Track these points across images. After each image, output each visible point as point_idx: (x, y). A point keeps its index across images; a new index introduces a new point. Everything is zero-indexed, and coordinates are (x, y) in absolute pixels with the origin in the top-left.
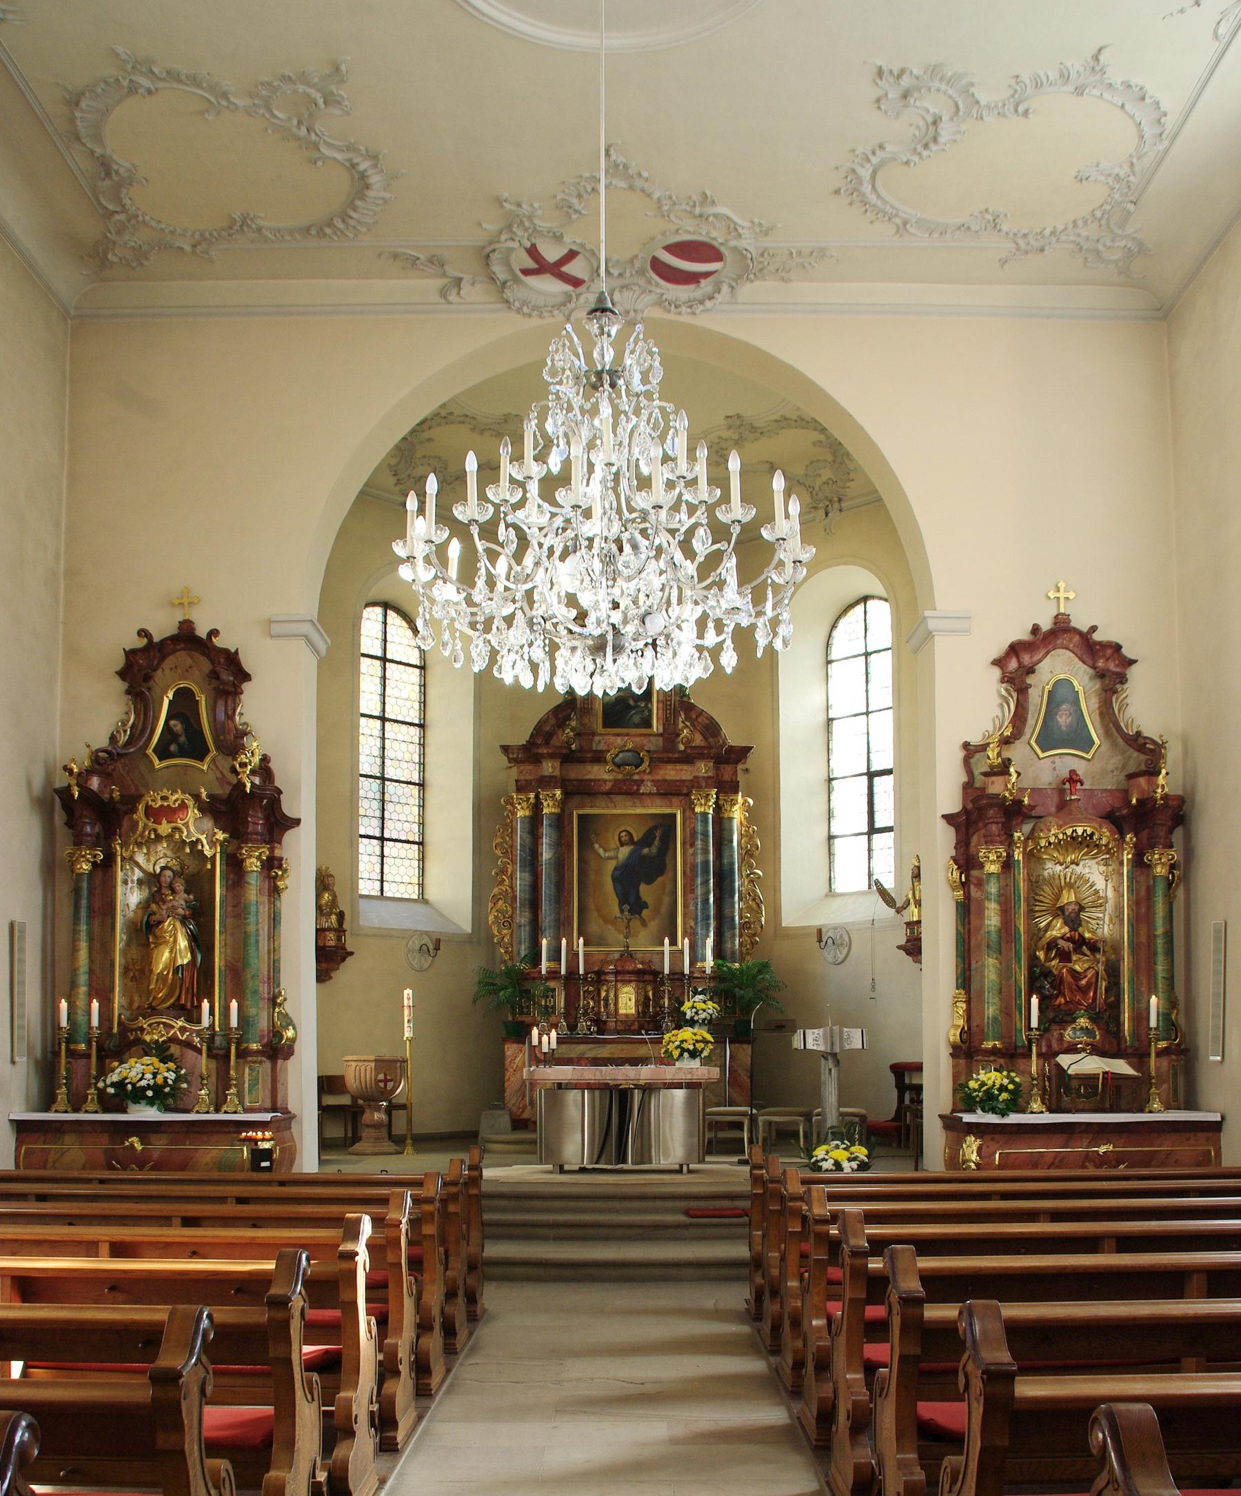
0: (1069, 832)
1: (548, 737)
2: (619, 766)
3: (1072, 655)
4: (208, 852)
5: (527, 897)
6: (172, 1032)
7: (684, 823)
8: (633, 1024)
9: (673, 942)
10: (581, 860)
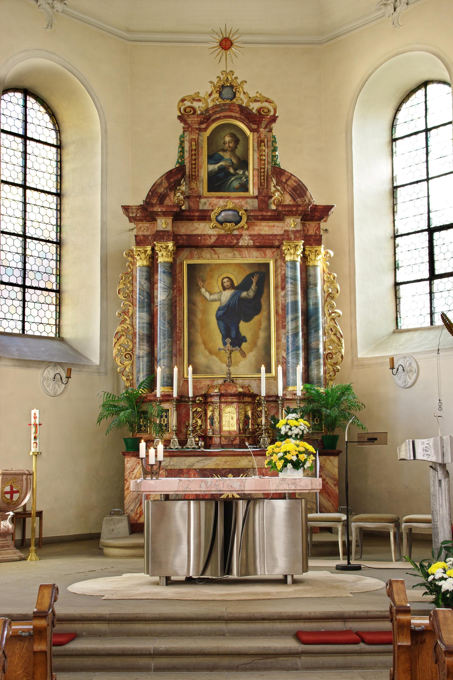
1: (162, 198)
2: (221, 223)
5: (145, 332)
7: (276, 271)
8: (235, 439)
9: (268, 370)
10: (191, 302)
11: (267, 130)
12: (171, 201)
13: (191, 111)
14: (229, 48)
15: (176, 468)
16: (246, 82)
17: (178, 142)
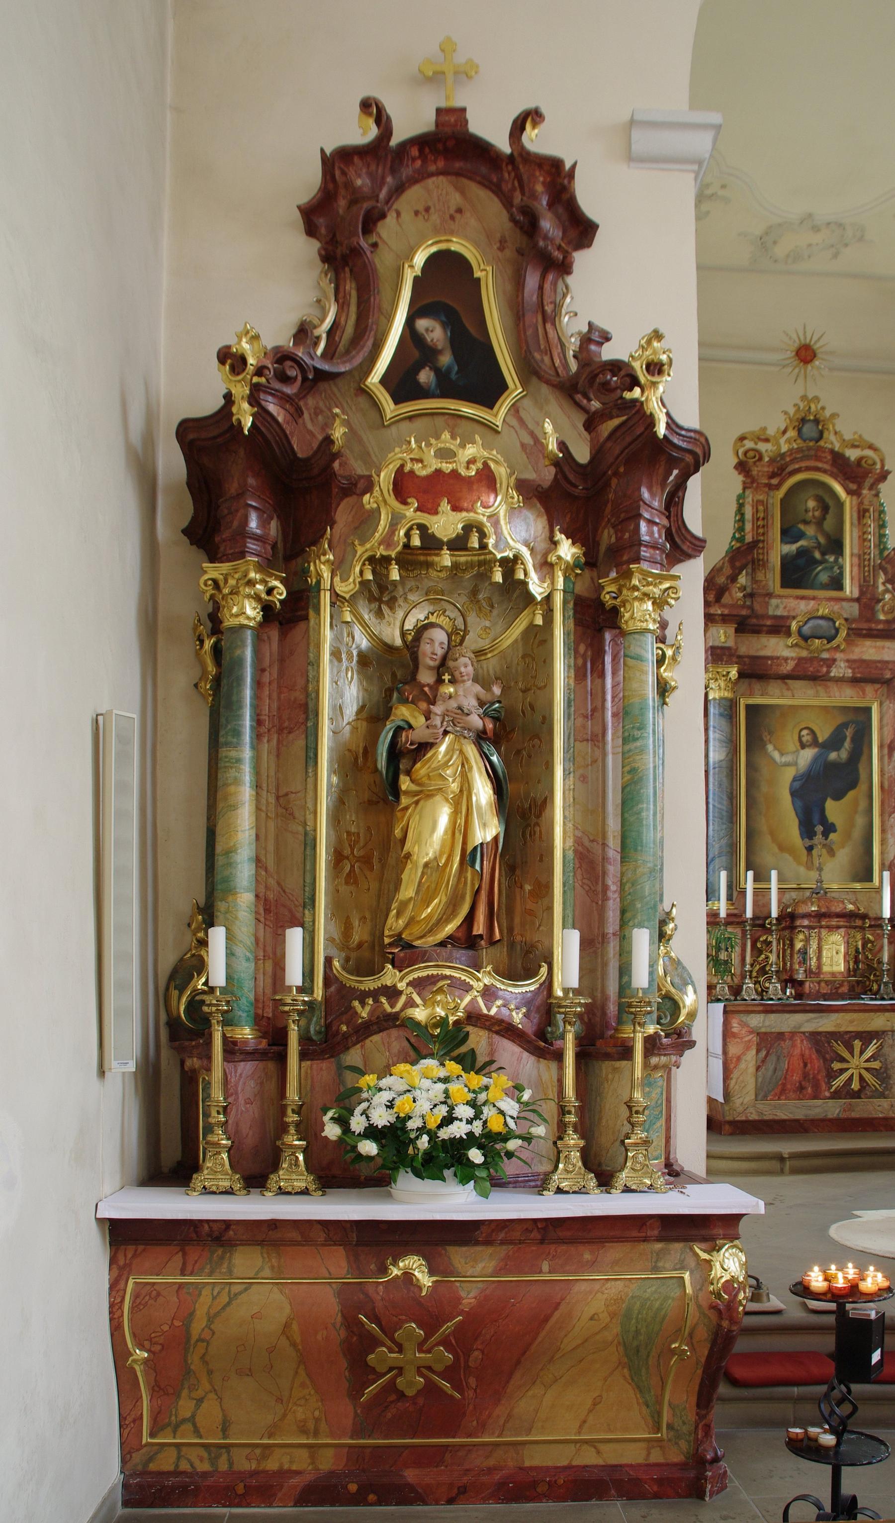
2: (806, 639)
4: (537, 588)
6: (468, 999)
10: (750, 765)
11: (873, 492)
12: (732, 598)
13: (755, 457)
14: (811, 361)
15: (773, 1030)
17: (734, 507)
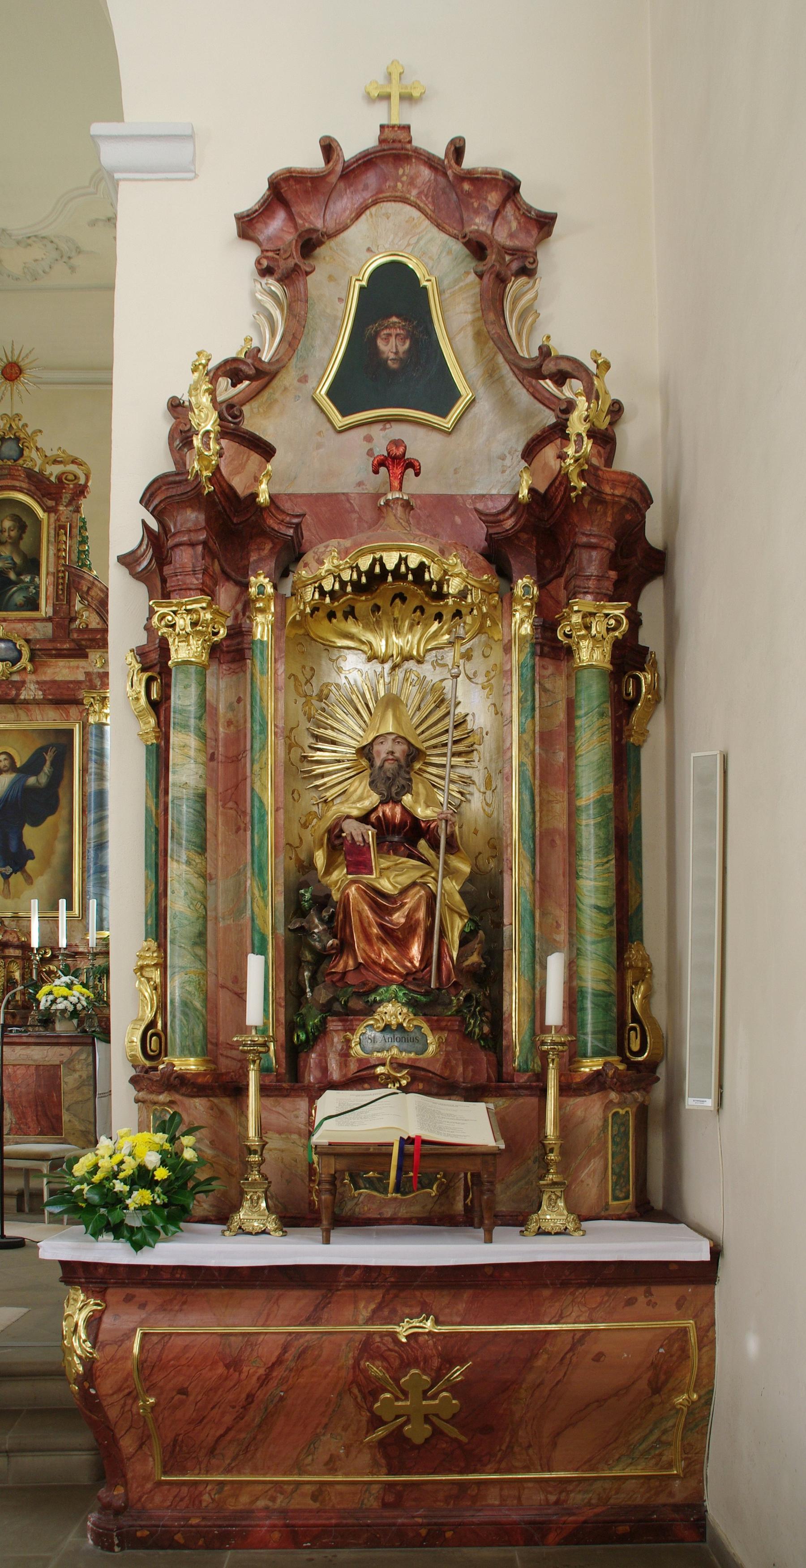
0: (365, 563)
3: (415, 213)
9: (70, 907)
11: (71, 508)
16: (40, 431)
